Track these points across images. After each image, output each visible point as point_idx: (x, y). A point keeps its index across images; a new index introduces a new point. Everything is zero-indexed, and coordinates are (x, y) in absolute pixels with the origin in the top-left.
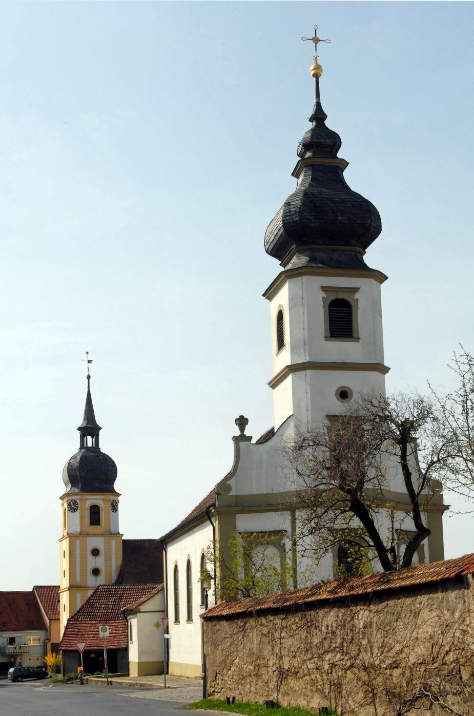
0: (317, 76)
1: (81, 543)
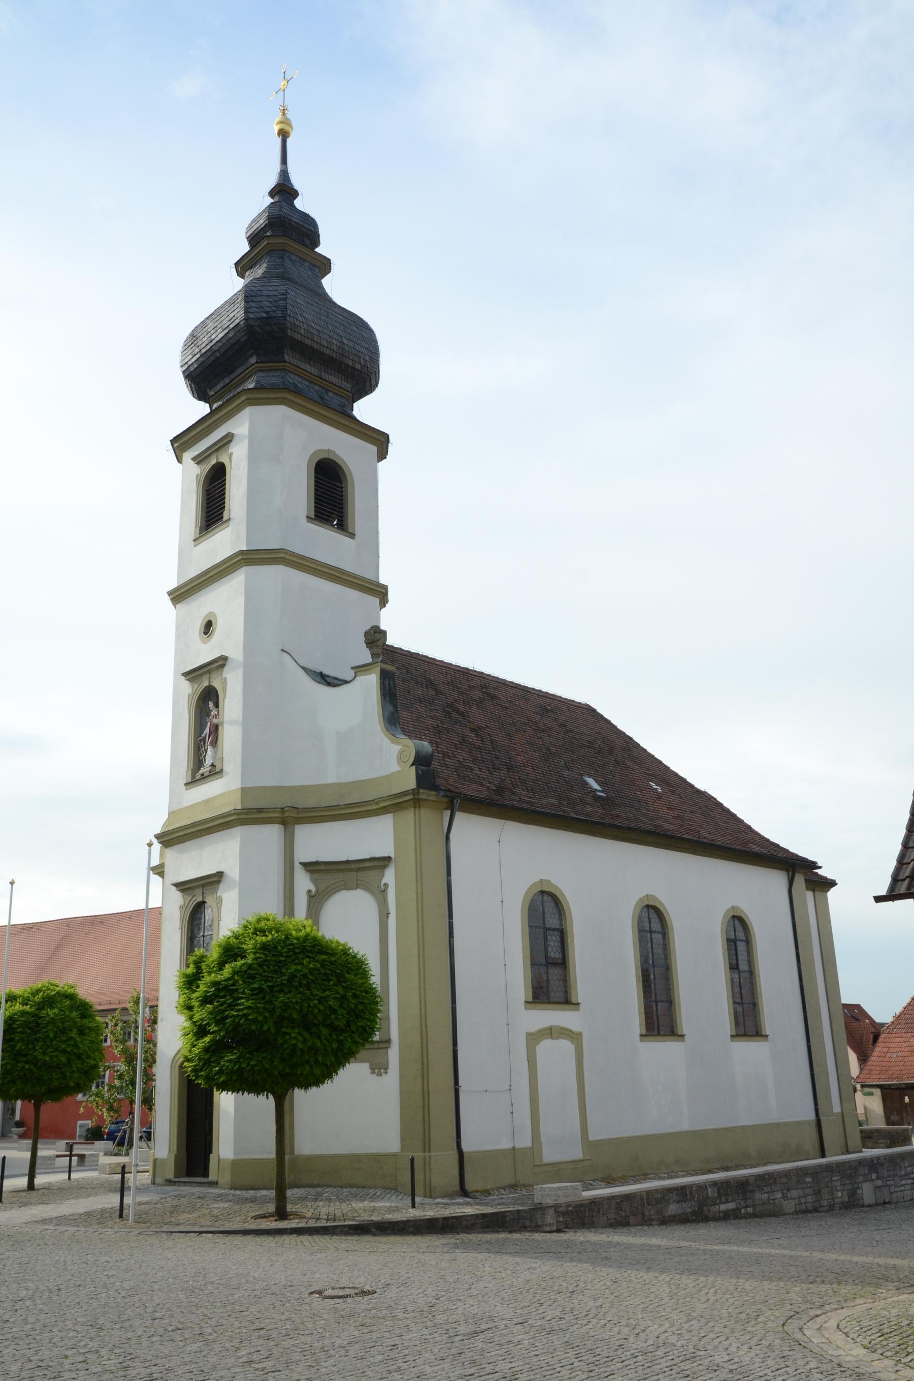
0: (284, 135)
1: (22, 1105)
